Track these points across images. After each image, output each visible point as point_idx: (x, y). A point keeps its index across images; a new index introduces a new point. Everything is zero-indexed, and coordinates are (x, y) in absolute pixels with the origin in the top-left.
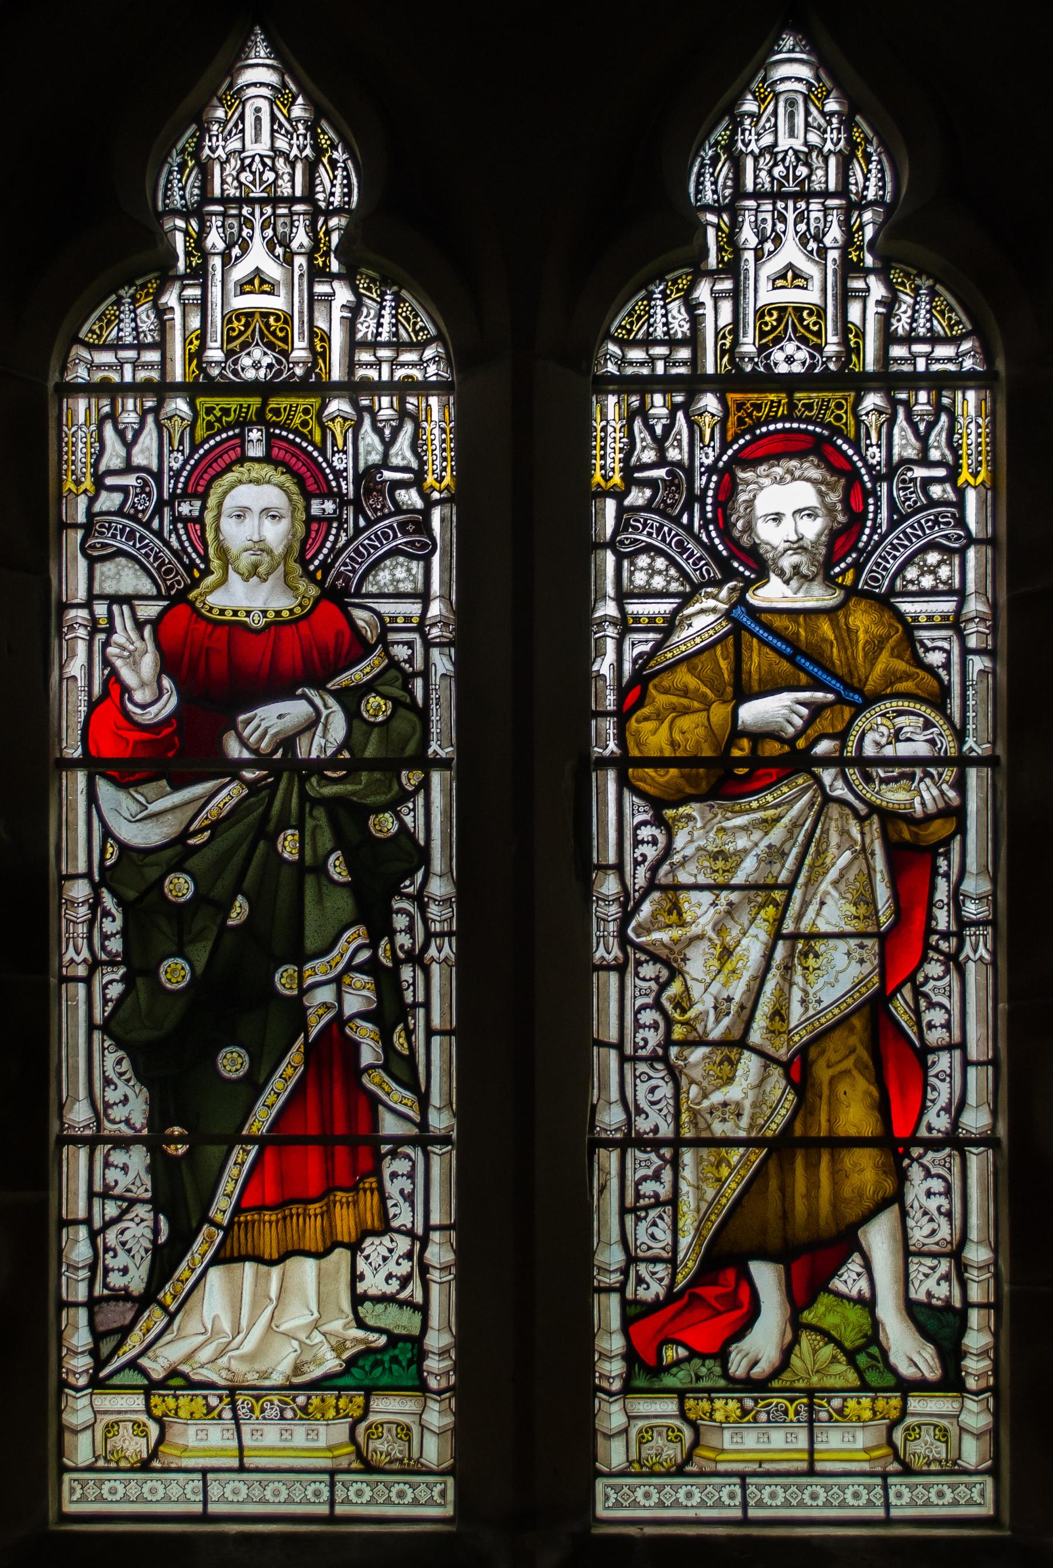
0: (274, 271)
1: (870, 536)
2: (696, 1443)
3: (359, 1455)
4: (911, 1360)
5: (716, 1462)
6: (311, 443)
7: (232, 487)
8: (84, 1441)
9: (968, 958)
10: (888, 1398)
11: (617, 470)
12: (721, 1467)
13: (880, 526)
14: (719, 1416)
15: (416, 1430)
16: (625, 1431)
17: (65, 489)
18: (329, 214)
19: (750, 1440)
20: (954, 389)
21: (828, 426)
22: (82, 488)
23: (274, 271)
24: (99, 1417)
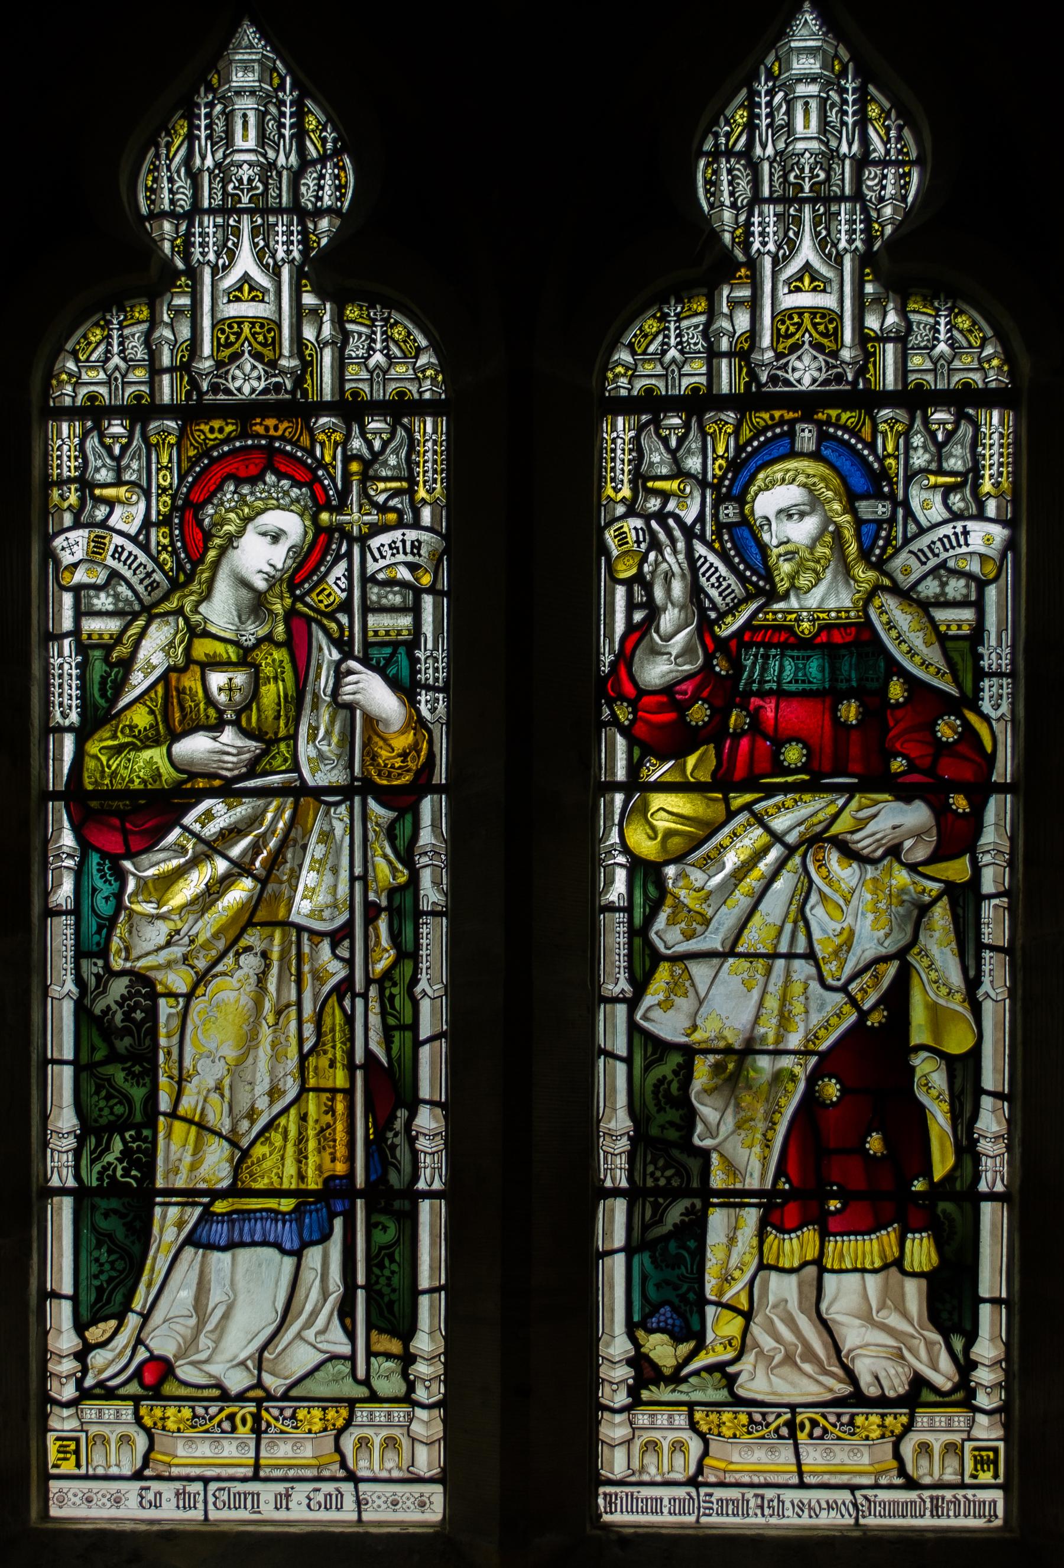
0: (262, 279)
1: (884, 549)
2: (706, 1453)
3: (902, 1471)
4: (877, 1378)
5: (170, 1465)
6: (860, 440)
7: (756, 495)
8: (620, 1455)
9: (425, 993)
10: (165, 1407)
11: (626, 481)
12: (175, 1471)
13: (895, 538)
14: (171, 1425)
15: (405, 1442)
16: (629, 1442)
17: (604, 496)
18: (318, 213)
19: (204, 1450)
20: (411, 414)
21: (199, 458)
22: (620, 496)
23: (262, 279)
24: (637, 1433)
